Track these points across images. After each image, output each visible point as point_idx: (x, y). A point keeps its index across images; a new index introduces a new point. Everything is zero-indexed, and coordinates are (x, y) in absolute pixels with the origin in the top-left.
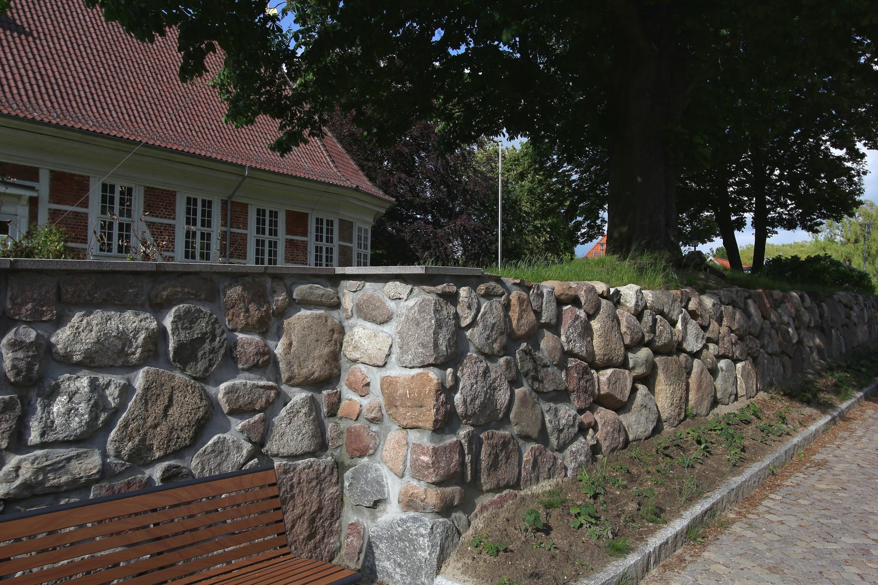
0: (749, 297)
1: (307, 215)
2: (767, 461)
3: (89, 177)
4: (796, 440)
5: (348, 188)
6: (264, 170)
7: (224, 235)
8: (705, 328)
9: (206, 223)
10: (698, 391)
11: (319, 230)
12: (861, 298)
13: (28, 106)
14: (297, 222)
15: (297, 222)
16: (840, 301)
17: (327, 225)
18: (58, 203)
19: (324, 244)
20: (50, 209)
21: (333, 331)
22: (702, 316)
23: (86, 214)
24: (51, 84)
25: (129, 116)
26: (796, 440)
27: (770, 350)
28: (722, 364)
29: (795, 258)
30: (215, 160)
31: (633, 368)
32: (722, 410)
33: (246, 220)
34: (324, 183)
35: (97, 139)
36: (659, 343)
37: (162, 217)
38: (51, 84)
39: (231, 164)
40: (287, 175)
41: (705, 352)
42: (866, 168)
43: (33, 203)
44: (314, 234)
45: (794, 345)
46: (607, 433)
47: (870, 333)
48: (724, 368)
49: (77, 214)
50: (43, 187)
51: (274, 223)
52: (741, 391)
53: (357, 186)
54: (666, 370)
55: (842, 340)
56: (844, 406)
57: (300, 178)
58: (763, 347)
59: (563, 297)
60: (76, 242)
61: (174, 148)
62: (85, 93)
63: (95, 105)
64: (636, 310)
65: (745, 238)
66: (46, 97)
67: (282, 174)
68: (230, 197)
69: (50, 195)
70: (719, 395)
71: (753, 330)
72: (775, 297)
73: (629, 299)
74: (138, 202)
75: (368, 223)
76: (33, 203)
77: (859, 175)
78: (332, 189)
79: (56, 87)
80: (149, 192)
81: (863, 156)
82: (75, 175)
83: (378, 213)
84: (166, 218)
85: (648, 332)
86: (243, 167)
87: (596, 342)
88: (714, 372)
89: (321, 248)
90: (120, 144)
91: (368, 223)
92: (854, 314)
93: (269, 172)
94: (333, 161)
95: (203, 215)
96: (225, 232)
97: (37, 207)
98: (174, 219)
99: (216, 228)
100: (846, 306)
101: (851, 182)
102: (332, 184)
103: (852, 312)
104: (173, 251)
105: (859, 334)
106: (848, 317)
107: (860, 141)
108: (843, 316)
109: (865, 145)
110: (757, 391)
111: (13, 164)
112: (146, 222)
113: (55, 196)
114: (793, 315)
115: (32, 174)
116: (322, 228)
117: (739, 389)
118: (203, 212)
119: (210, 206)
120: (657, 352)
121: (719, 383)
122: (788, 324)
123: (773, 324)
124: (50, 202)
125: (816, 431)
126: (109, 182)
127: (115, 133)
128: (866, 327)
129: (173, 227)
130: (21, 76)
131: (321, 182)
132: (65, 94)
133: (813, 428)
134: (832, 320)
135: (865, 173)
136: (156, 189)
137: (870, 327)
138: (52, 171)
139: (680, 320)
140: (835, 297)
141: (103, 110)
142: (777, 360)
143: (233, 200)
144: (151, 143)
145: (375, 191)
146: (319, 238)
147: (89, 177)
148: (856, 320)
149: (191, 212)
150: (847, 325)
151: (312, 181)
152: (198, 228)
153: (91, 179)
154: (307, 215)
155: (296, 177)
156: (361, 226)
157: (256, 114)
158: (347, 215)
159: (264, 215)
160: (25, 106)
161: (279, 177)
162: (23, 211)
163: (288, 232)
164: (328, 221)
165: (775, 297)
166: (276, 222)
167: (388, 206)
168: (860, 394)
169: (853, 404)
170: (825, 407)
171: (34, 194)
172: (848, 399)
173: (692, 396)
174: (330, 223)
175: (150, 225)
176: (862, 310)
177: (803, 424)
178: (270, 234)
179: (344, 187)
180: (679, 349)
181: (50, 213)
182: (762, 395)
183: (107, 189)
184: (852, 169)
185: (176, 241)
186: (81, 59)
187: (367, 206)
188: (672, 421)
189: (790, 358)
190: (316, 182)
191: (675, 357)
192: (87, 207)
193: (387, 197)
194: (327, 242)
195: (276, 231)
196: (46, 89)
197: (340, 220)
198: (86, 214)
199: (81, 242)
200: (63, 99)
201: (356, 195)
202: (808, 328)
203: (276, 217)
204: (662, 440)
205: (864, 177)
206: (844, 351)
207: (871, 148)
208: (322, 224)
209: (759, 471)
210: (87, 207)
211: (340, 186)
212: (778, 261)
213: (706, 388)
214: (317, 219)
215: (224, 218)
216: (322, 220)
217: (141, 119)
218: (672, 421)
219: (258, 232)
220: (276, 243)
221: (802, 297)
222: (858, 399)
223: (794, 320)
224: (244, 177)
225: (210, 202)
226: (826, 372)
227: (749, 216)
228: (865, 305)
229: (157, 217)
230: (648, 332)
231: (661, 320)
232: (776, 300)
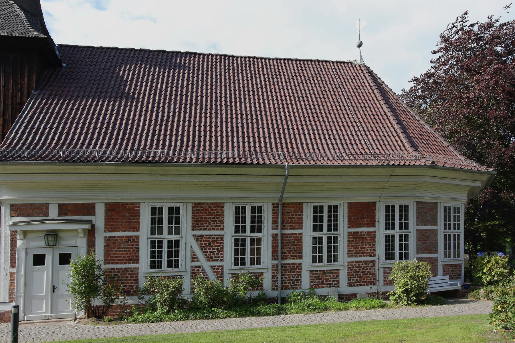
3: (139, 204)
5: (420, 166)
7: (275, 237)
9: (404, 226)
11: (447, 218)
13: (329, 155)
14: (362, 213)
15: (362, 213)
18: (113, 231)
19: (452, 232)
20: (105, 237)
21: (506, 328)
23: (436, 231)
33: (300, 220)
37: (210, 230)
43: (91, 233)
44: (443, 222)
49: (129, 238)
50: (99, 219)
53: (433, 163)
60: (129, 263)
62: (351, 131)
68: (281, 199)
74: (186, 218)
76: (91, 233)
78: (397, 171)
82: (127, 204)
83: (473, 188)
84: (214, 229)
89: (450, 236)
91: (461, 200)
96: (277, 235)
97: (94, 237)
98: (222, 229)
99: (268, 231)
102: (399, 166)
104: (221, 260)
111: (73, 204)
112: (194, 236)
113: (110, 226)
115: (89, 209)
116: (450, 216)
119: (336, 211)
126: (157, 204)
127: (371, 162)
129: (374, 234)
136: (204, 204)
138: (106, 204)
143: (284, 201)
146: (447, 226)
147: (139, 204)
152: (325, 234)
160: (353, 156)
162: (82, 242)
166: (336, 217)
167: (485, 178)
174: (404, 208)
175: (197, 238)
181: (105, 241)
185: (225, 250)
193: (483, 168)
194: (455, 229)
198: (138, 237)
199: (133, 263)
201: (432, 172)
215: (275, 221)
229: (205, 229)
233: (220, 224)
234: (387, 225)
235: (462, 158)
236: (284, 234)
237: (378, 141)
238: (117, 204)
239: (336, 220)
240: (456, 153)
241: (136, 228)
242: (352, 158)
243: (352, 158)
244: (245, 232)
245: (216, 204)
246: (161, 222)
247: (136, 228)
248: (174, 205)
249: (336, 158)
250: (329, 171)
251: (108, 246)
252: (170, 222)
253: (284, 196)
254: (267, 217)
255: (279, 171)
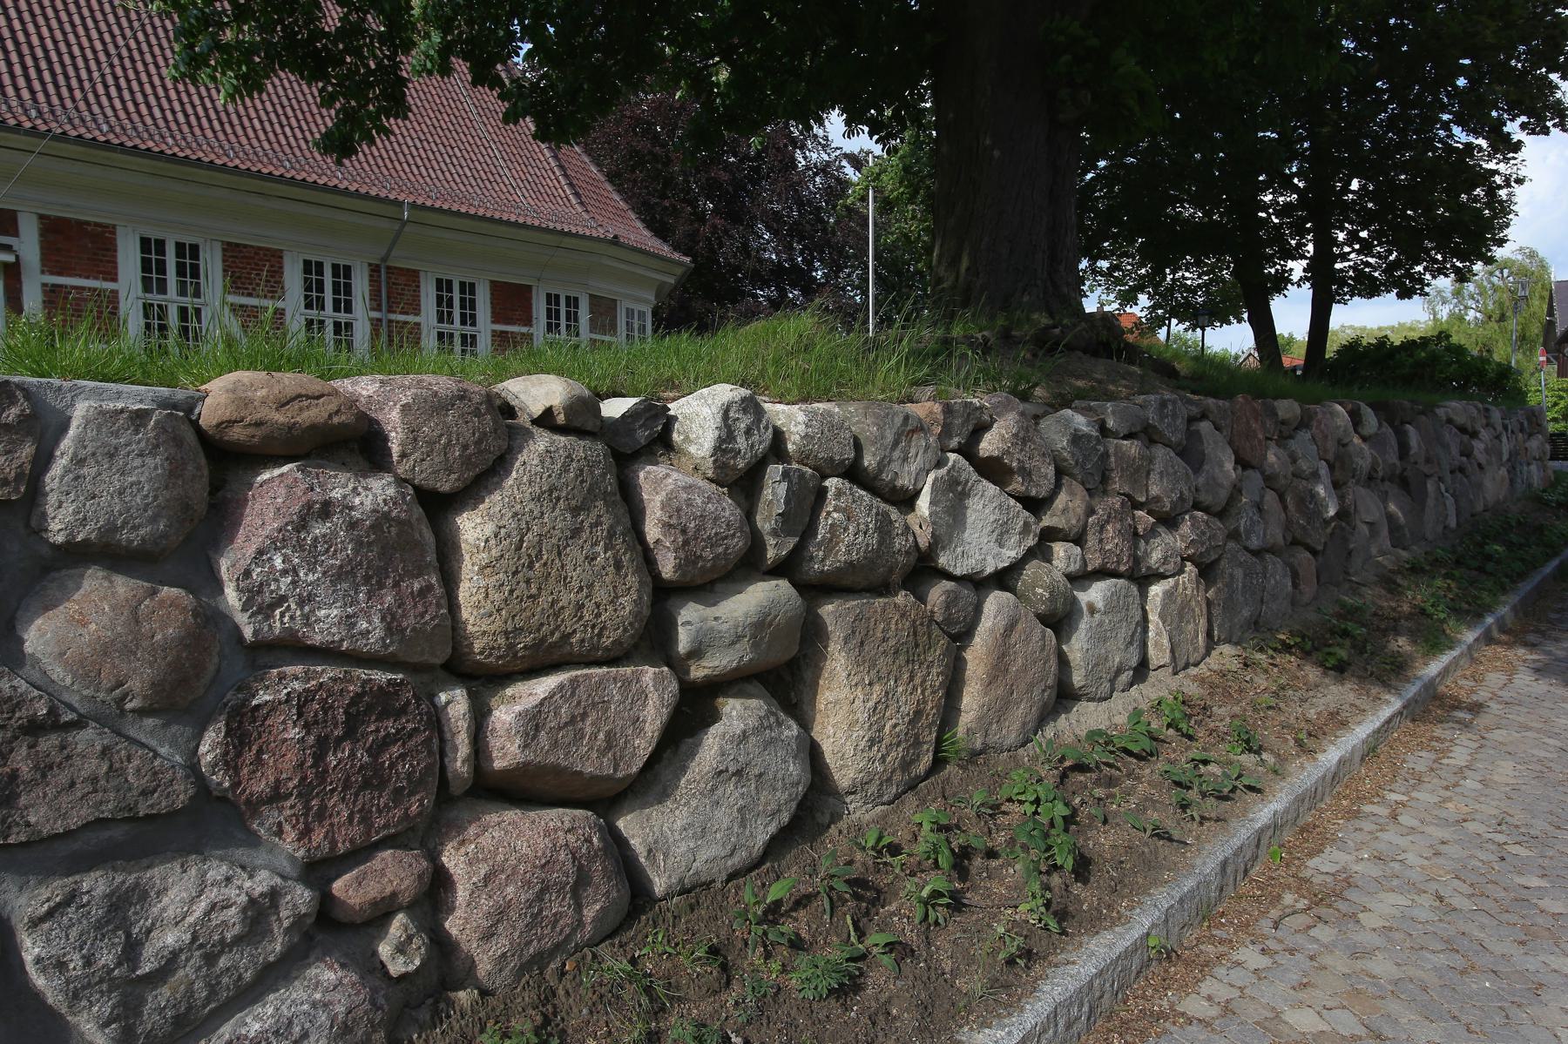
0: (1204, 416)
1: (530, 287)
2: (1142, 921)
3: (114, 226)
4: (1264, 812)
5: (598, 239)
6: (440, 210)
8: (1035, 505)
9: (469, 319)
10: (991, 682)
12: (1496, 415)
16: (1450, 421)
17: (568, 305)
18: (60, 274)
20: (44, 285)
22: (1026, 473)
23: (115, 293)
24: (35, 59)
25: (187, 116)
26: (1264, 812)
27: (1255, 543)
28: (1095, 594)
29: (1382, 342)
30: (346, 192)
31: (696, 653)
32: (1085, 718)
34: (554, 231)
35: (114, 155)
36: (822, 562)
38: (35, 59)
39: (377, 198)
40: (483, 218)
41: (1031, 570)
42: (1522, 173)
45: (1327, 522)
46: (500, 914)
47: (1512, 481)
48: (1100, 605)
50: (28, 245)
51: (469, 304)
52: (1158, 654)
53: (616, 237)
54: (859, 641)
55: (1450, 501)
56: (1434, 668)
57: (508, 223)
58: (1234, 535)
59: (237, 434)
61: (352, 189)
63: (242, 124)
64: (720, 466)
65: (1291, 314)
66: (21, 82)
67: (475, 217)
68: (384, 260)
69: (42, 260)
70: (1077, 679)
71: (1205, 498)
72: (1281, 414)
73: (695, 430)
74: (212, 264)
75: (646, 301)
77: (1508, 185)
78: (567, 242)
79: (43, 65)
80: (497, 289)
81: (1517, 146)
82: (88, 223)
83: (664, 283)
85: (774, 533)
86: (398, 204)
87: (469, 589)
88: (1059, 620)
90: (160, 164)
92: (1478, 446)
93: (449, 212)
94: (577, 195)
95: (336, 291)
96: (380, 320)
97: (20, 281)
99: (361, 317)
100: (1462, 430)
101: (1492, 191)
102: (569, 234)
103: (1475, 443)
105: (1488, 484)
106: (1467, 453)
107: (1512, 120)
108: (1455, 451)
109: (1523, 126)
110: (1211, 643)
113: (53, 260)
114: (1330, 456)
117: (1151, 651)
118: (336, 286)
119: (348, 275)
120: (816, 590)
121: (1077, 647)
122: (1315, 475)
123: (1269, 480)
124: (43, 272)
125: (1342, 762)
126: (154, 234)
128: (1503, 472)
130: (116, 78)
131: (547, 230)
132: (61, 79)
133: (1331, 756)
134: (1428, 461)
135: (1520, 181)
136: (245, 246)
137: (1512, 470)
138: (41, 217)
139: (927, 490)
140: (1440, 412)
141: (136, 105)
142: (1275, 565)
144: (363, 191)
145: (665, 250)
147: (114, 226)
148: (1482, 458)
149: (312, 287)
150: (1462, 470)
151: (532, 227)
153: (119, 230)
154: (530, 287)
155: (500, 221)
156: (631, 306)
157: (268, 71)
158: (605, 288)
159: (450, 290)
161: (467, 222)
163: (497, 317)
164: (568, 298)
165: (1281, 414)
166: (473, 302)
167: (679, 271)
168: (1469, 636)
169: (1455, 662)
170: (1392, 672)
171: (11, 258)
172: (1442, 652)
173: (971, 701)
176: (1498, 437)
177: (1308, 740)
178: (463, 322)
179: (590, 238)
180: (922, 569)
181: (45, 292)
182: (1226, 656)
183: (151, 248)
184: (1496, 172)
186: (99, 16)
187: (640, 271)
188: (873, 789)
189: (1314, 552)
190: (539, 229)
191: (902, 598)
192: (115, 280)
193: (676, 256)
195: (473, 317)
196: (206, 110)
197: (591, 296)
200: (57, 87)
201: (613, 250)
202: (1371, 479)
203: (472, 292)
204: (835, 851)
205: (1517, 189)
206: (1453, 523)
207: (1533, 132)
208: (557, 304)
209: (1100, 973)
210: (115, 280)
211: (583, 237)
212: (1353, 349)
213: (1024, 668)
214: (549, 296)
215: (375, 295)
216: (557, 297)
217: (210, 121)
218: (873, 789)
219: (441, 320)
220: (473, 337)
221: (1355, 416)
222: (1470, 647)
223: (1331, 467)
224: (404, 223)
225: (348, 269)
226: (1404, 577)
227: (1297, 268)
228: (1505, 427)
229: (250, 295)
230: (774, 533)
231: (839, 493)
232: (1283, 423)
233: (275, 287)
234: (549, 325)
235: (646, 233)
236: (390, 321)
237: (272, 124)
238: (66, 221)
239: (473, 307)
240: (639, 224)
241: (109, 273)
242: (194, 145)
243: (194, 145)
244: (165, 293)
245: (268, 249)
246: (162, 269)
247: (109, 273)
248: (188, 240)
249: (105, 128)
250: (467, 223)
251: (50, 302)
252: (181, 271)
253: (393, 253)
254: (361, 285)
255: (390, 211)
